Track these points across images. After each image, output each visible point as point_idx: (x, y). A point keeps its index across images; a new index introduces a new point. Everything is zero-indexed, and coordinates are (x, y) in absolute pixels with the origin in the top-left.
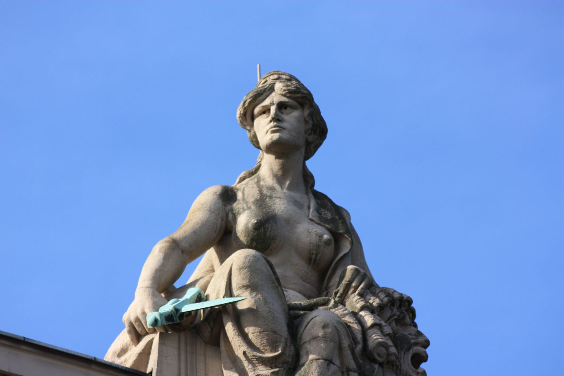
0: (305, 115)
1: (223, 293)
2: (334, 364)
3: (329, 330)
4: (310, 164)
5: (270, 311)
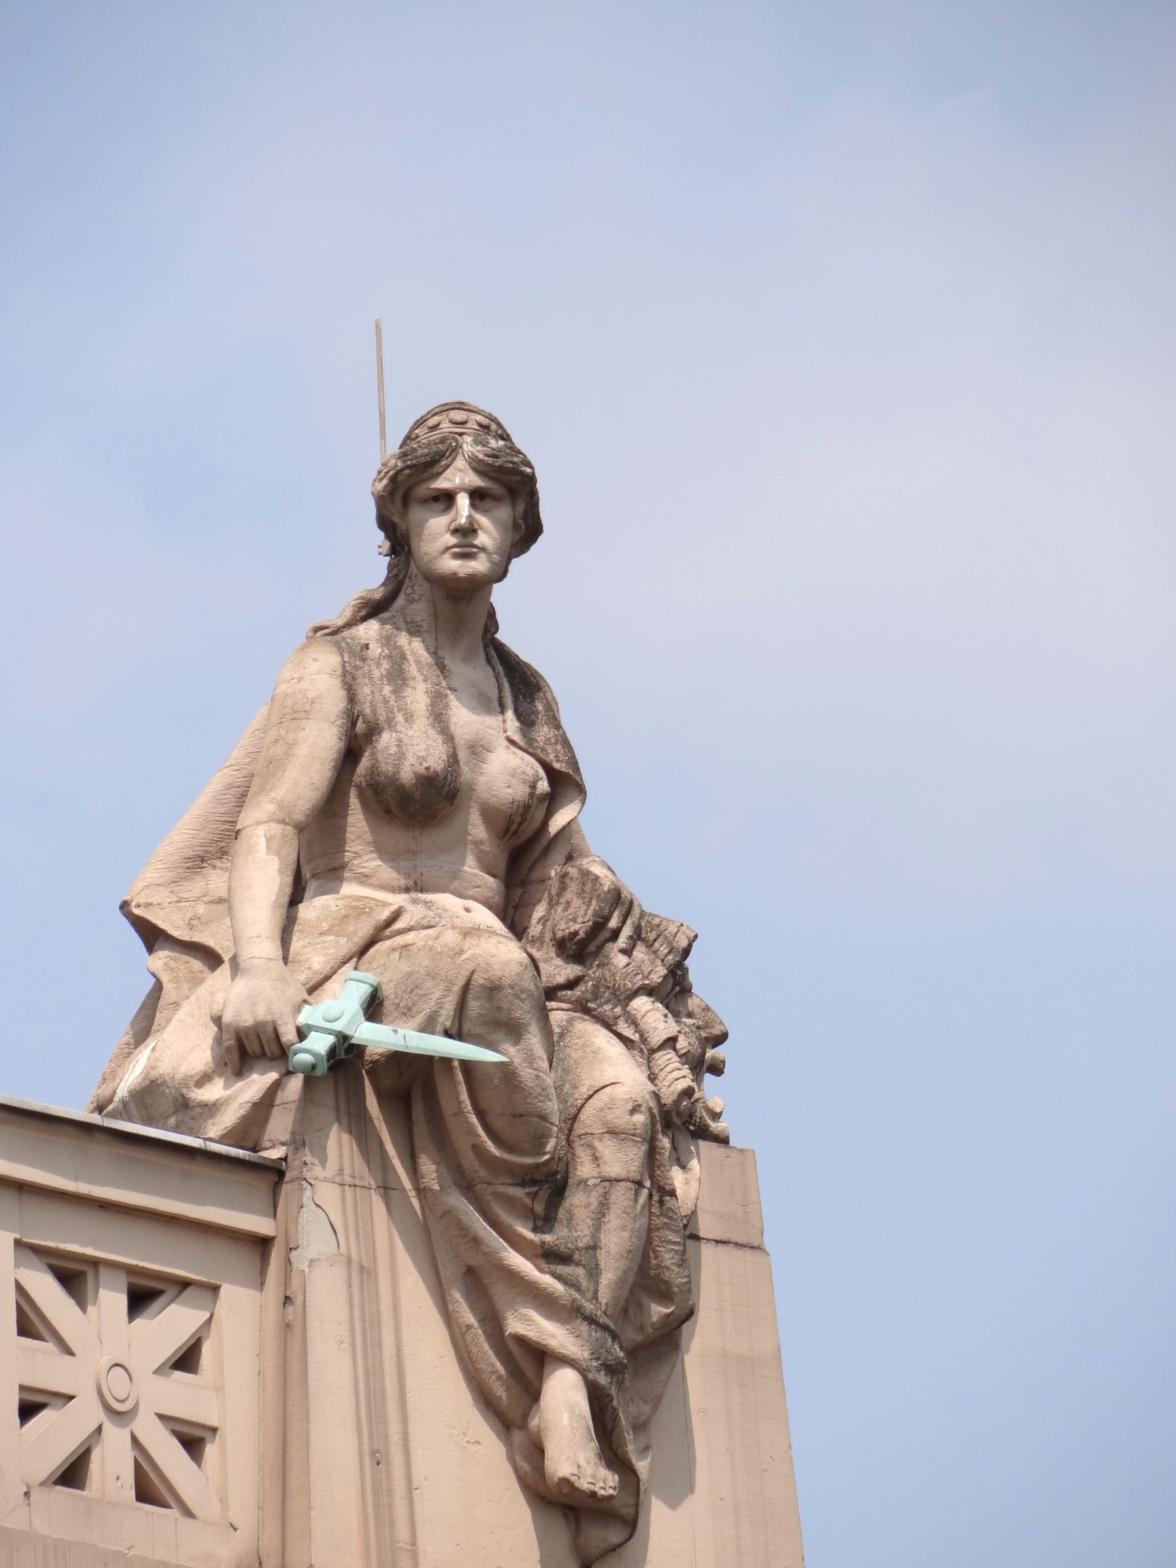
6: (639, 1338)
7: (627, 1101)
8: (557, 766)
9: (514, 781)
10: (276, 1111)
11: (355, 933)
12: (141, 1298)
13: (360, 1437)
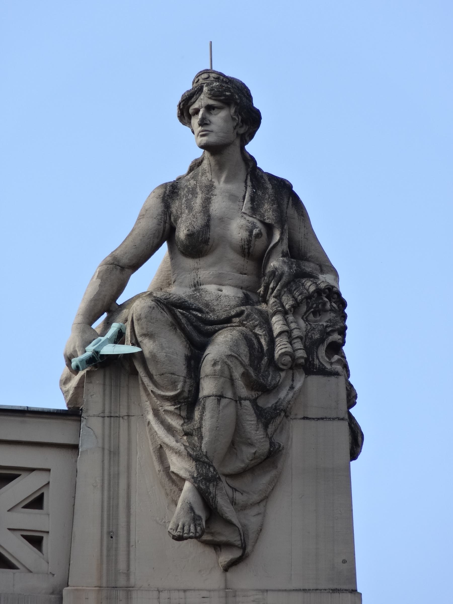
0: (232, 114)
3: (218, 367)
4: (250, 148)
5: (166, 356)
6: (243, 465)
9: (242, 231)
13: (102, 526)
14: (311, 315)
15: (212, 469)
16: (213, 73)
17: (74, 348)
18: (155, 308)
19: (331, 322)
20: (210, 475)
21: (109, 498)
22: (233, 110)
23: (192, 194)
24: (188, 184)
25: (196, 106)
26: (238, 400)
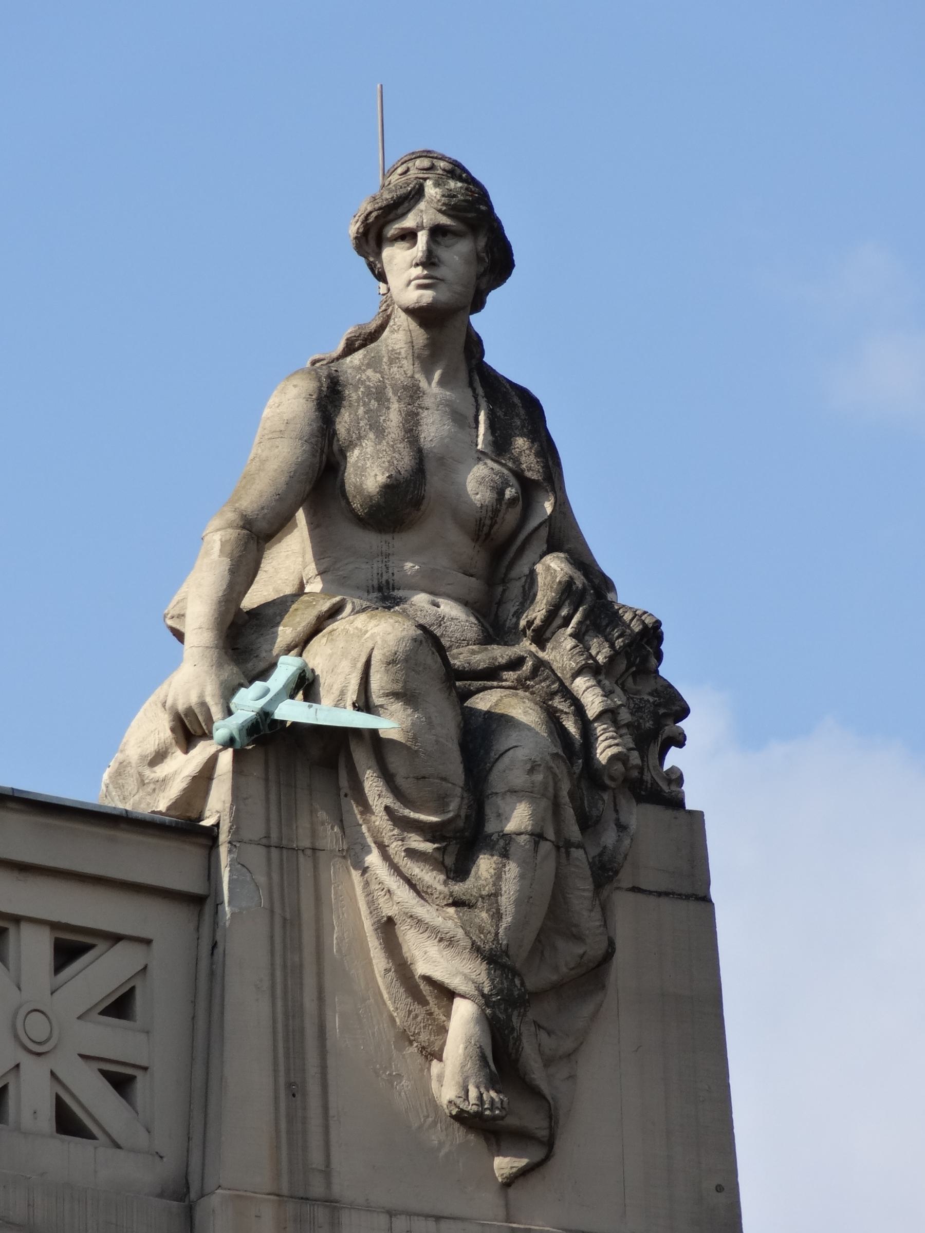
1: (352, 695)
2: (547, 840)
3: (539, 777)
4: (478, 321)
5: (437, 742)
6: (555, 978)
7: (526, 762)
8: (529, 474)
9: (481, 488)
10: (215, 783)
11: (299, 623)
12: (69, 949)
13: (276, 1071)
14: (630, 680)
15: (517, 982)
16: (440, 159)
17: (201, 695)
18: (424, 644)
19: (659, 697)
20: (516, 993)
21: (286, 1014)
22: (482, 242)
23: (378, 400)
24: (364, 377)
25: (409, 222)
26: (563, 846)
